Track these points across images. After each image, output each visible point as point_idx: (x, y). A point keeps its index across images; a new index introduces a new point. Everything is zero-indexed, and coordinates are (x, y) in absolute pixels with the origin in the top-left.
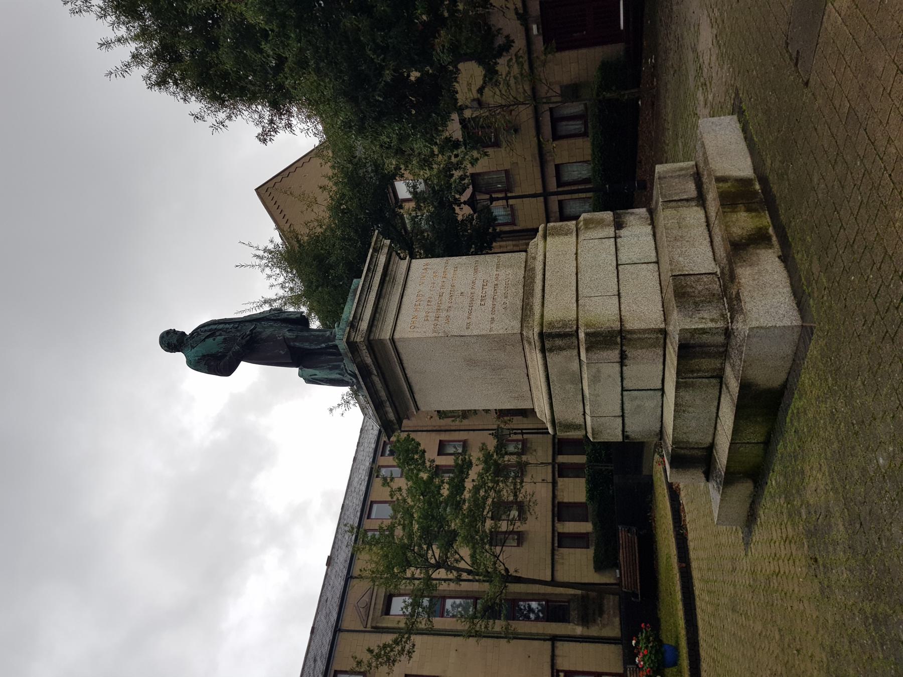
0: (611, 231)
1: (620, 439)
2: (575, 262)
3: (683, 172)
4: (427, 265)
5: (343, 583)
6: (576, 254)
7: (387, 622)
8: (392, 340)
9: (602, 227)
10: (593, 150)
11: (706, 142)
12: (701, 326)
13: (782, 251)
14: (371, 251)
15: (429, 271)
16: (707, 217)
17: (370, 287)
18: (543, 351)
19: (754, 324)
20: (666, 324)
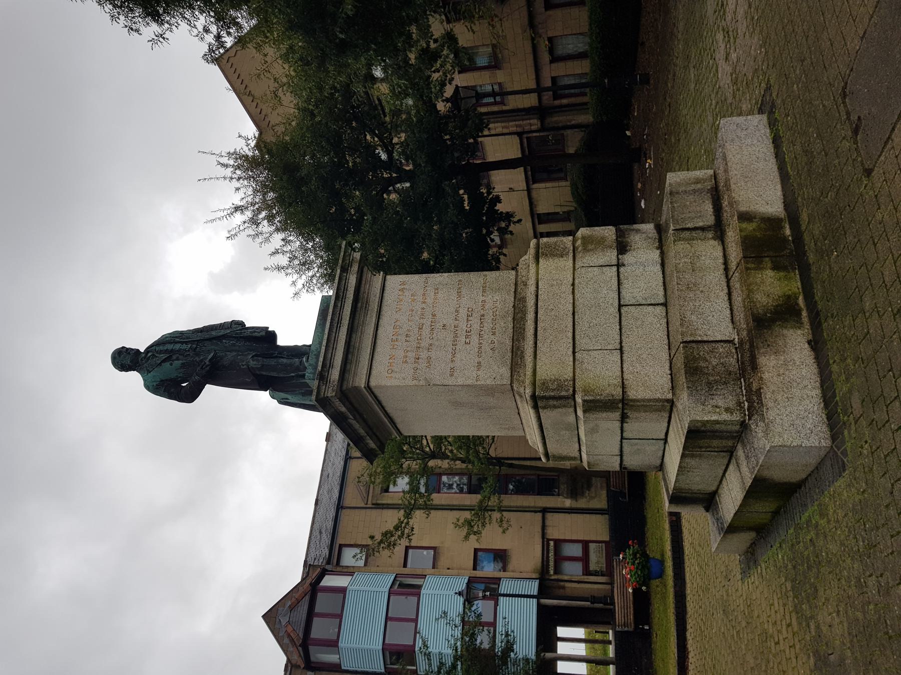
0: (611, 256)
1: (618, 469)
2: (571, 296)
3: (699, 186)
4: (403, 283)
5: (342, 463)
6: (573, 285)
7: (387, 499)
8: (368, 387)
10: (590, 25)
11: (730, 156)
12: (714, 418)
13: (813, 334)
14: (339, 271)
16: (725, 256)
18: (536, 407)
19: (777, 441)
20: (674, 394)
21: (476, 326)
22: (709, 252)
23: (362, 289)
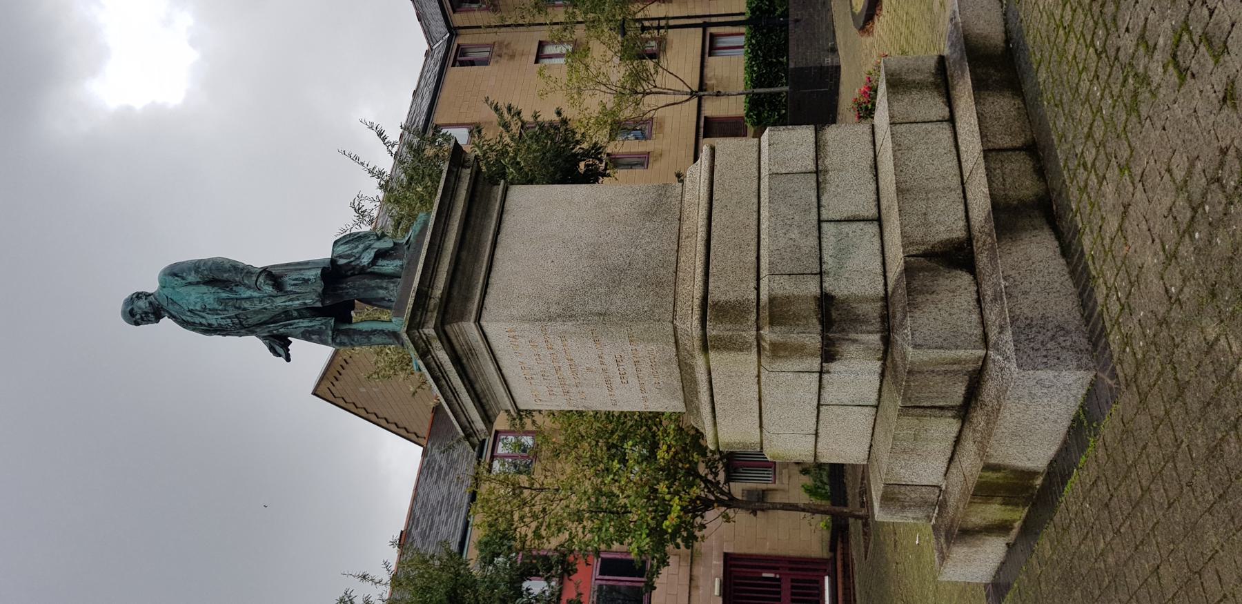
0: (815, 364)
3: (955, 367)
6: (759, 376)
23: (458, 347)
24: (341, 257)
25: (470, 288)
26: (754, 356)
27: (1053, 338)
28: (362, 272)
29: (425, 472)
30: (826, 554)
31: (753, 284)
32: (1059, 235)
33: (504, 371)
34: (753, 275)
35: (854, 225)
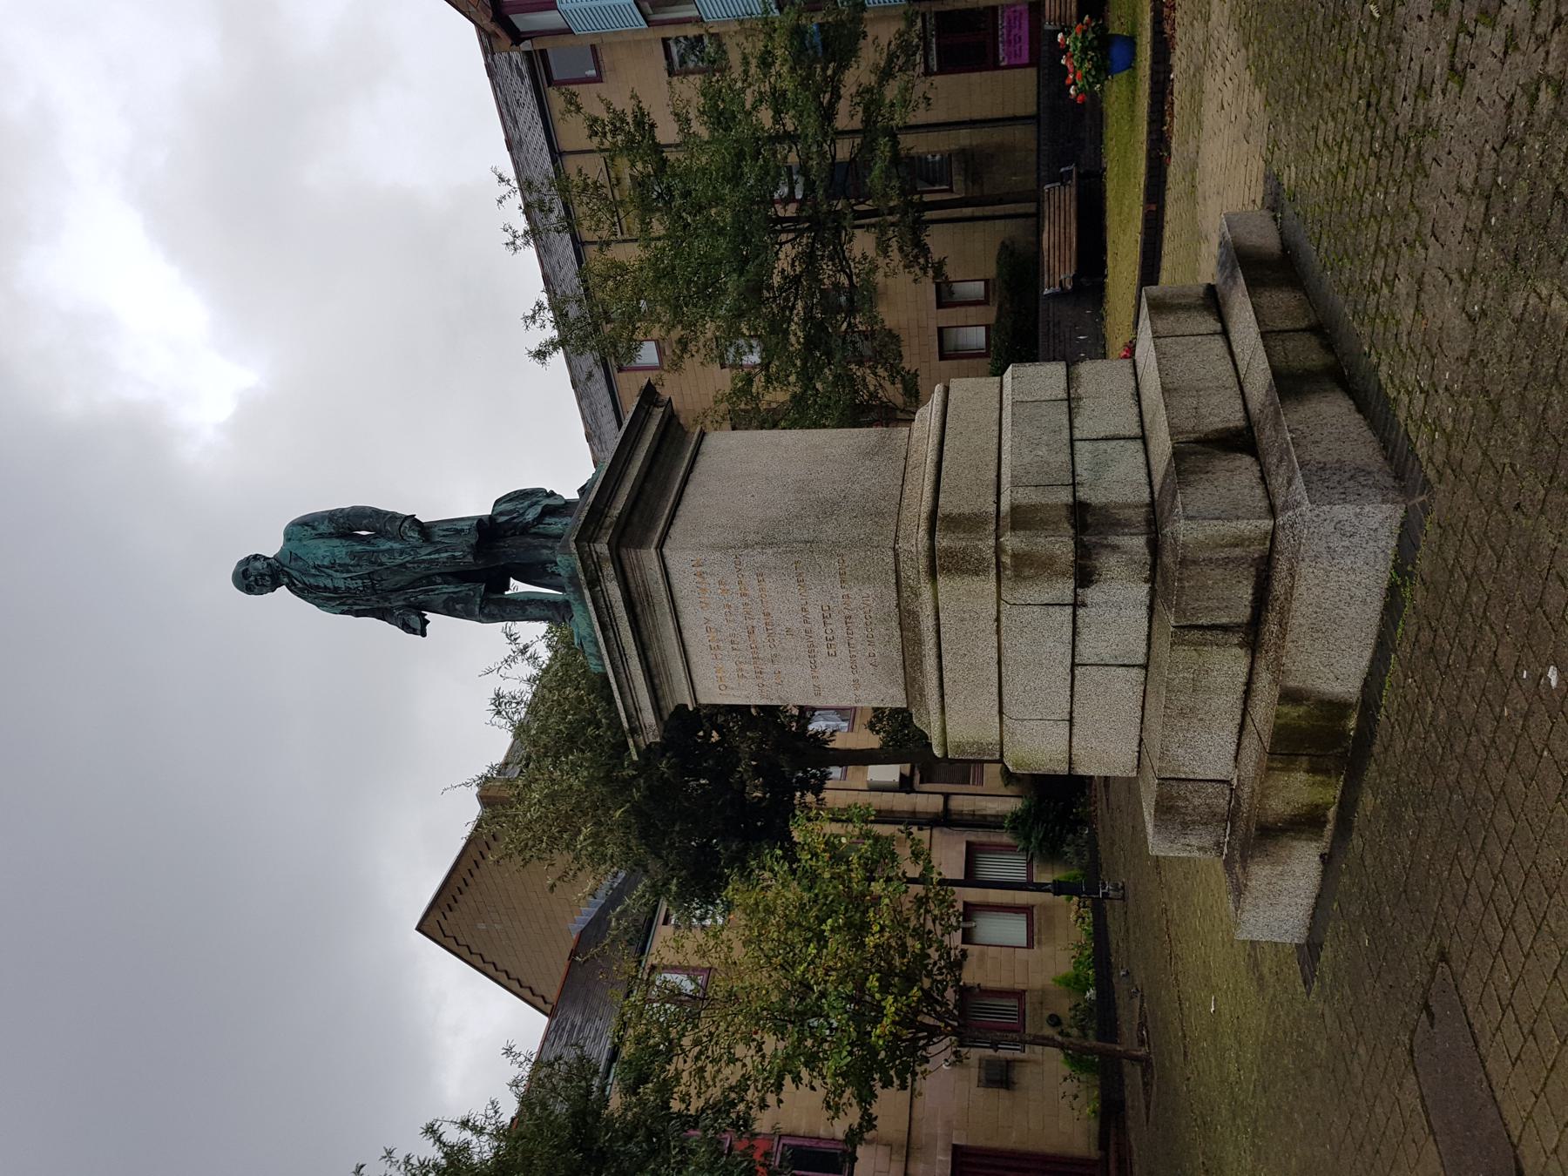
0: (1064, 589)
2: (995, 638)
3: (1238, 551)
6: (998, 620)
9: (1049, 579)
13: (1332, 848)
15: (710, 580)
17: (623, 654)
21: (841, 632)
22: (1229, 663)
23: (632, 586)
24: (501, 514)
25: (653, 520)
26: (992, 585)
27: (1352, 478)
28: (525, 529)
29: (552, 1037)
30: (1095, 1154)
31: (993, 498)
32: (1352, 394)
33: (685, 635)
34: (992, 490)
35: (1114, 443)
